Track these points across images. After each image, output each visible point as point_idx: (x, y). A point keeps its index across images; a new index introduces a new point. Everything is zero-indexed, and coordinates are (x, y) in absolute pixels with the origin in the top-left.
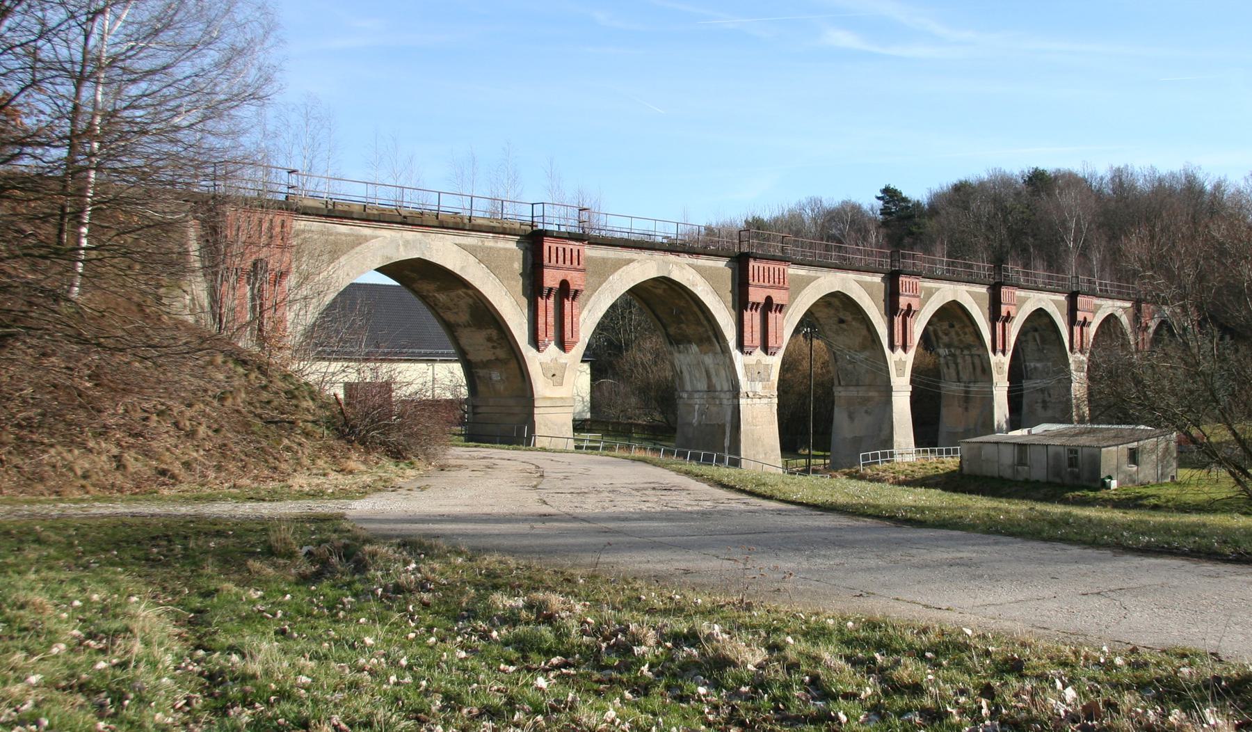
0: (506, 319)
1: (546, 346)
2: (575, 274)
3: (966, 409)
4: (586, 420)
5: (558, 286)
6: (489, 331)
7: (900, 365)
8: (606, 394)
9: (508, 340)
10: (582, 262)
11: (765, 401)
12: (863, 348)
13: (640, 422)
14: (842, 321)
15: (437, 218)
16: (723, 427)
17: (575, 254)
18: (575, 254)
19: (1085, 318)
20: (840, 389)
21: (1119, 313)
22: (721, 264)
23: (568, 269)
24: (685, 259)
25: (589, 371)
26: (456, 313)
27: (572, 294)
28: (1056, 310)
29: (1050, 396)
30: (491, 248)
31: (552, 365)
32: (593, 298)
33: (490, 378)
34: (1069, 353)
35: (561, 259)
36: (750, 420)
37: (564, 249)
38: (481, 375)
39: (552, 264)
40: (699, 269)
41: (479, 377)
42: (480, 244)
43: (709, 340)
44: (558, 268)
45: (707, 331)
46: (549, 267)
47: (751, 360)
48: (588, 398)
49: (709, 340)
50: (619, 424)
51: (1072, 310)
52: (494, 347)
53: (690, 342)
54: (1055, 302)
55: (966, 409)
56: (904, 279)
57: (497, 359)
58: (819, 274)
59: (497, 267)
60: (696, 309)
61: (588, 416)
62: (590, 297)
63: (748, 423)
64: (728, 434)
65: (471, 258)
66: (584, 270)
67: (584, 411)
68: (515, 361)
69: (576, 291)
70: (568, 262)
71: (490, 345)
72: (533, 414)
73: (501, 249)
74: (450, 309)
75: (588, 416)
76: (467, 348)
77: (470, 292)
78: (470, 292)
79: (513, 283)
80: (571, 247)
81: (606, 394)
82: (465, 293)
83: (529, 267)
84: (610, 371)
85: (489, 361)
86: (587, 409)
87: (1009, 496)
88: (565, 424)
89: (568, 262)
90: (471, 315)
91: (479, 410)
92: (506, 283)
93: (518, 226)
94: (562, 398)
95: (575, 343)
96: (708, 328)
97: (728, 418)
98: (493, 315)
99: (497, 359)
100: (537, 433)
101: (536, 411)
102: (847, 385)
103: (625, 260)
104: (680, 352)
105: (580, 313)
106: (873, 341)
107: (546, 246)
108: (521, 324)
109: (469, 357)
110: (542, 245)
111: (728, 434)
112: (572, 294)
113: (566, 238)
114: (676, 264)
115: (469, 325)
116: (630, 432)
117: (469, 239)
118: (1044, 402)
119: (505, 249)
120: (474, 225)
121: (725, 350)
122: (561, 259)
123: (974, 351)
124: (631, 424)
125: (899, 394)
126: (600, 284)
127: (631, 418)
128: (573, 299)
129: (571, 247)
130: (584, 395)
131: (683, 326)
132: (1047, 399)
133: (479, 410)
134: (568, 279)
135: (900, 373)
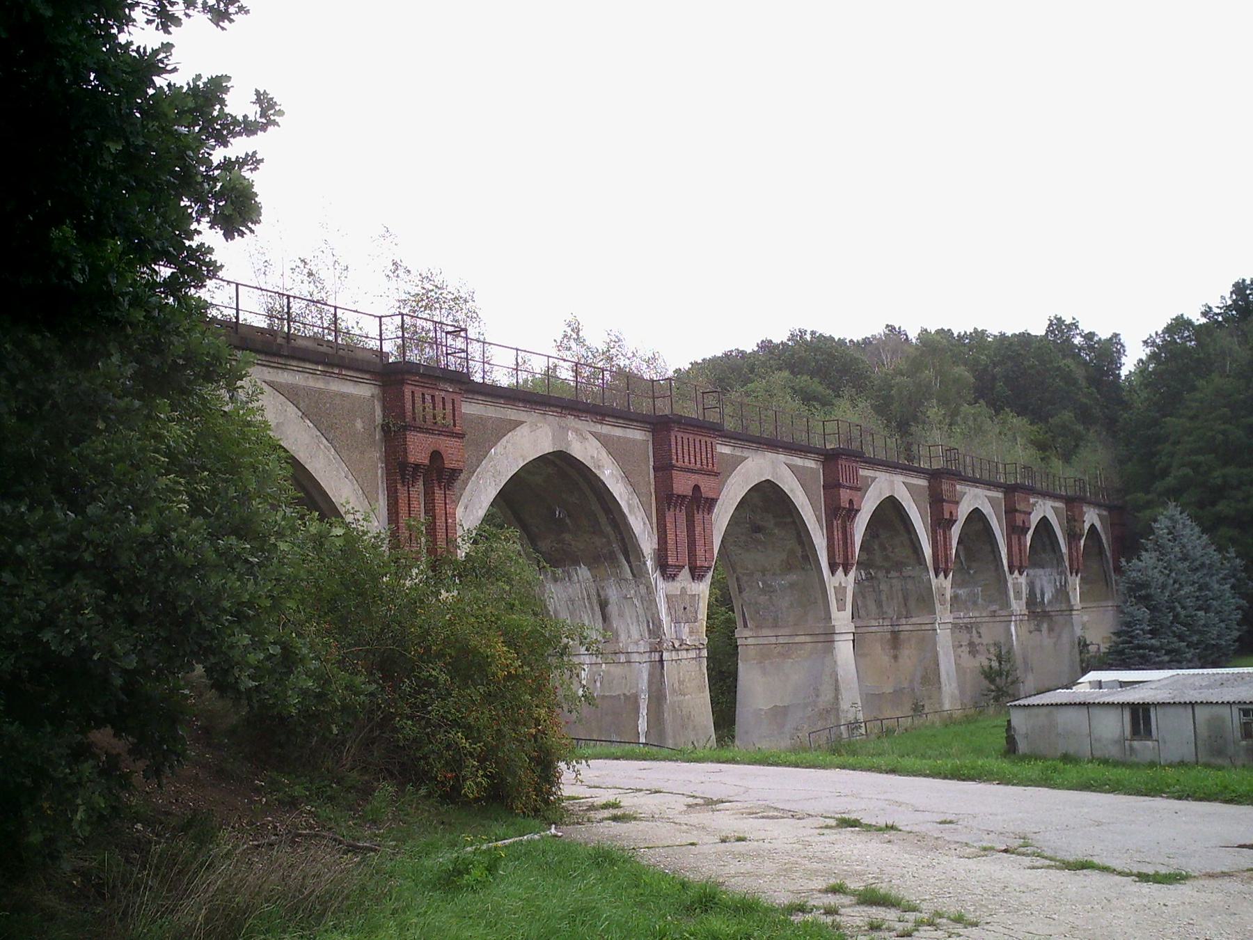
3: (896, 657)
7: (840, 590)
11: (693, 654)
12: (788, 567)
14: (757, 529)
15: (236, 332)
16: (634, 700)
19: (696, 488)
20: (747, 633)
21: (987, 510)
22: (637, 435)
24: (587, 425)
28: (604, 456)
29: (980, 637)
34: (1007, 573)
36: (676, 685)
39: (680, 464)
40: (605, 441)
43: (612, 558)
45: (609, 543)
47: (674, 587)
49: (612, 558)
51: (1011, 511)
53: (576, 562)
54: (990, 499)
55: (896, 657)
56: (844, 463)
58: (746, 453)
60: (595, 507)
63: (674, 691)
64: (644, 711)
65: (291, 409)
87: (1150, 717)
96: (612, 538)
97: (644, 684)
102: (759, 627)
104: (556, 580)
106: (806, 558)
107: (407, 391)
111: (644, 711)
114: (576, 431)
118: (971, 644)
120: (294, 348)
121: (639, 573)
123: (908, 571)
131: (567, 537)
132: (977, 641)
134: (442, 449)
135: (841, 608)
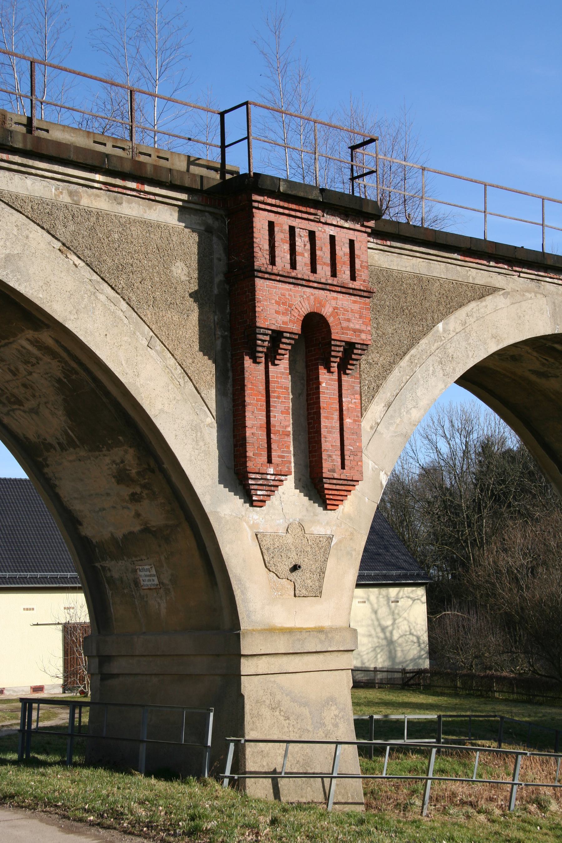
0: (151, 412)
1: (272, 488)
2: (345, 301)
4: (425, 671)
5: (297, 328)
6: (118, 453)
8: (451, 631)
9: (163, 471)
10: (362, 274)
13: (505, 674)
17: (343, 250)
18: (343, 250)
23: (324, 287)
25: (424, 599)
26: (35, 411)
27: (337, 352)
30: (99, 214)
31: (289, 539)
32: (396, 373)
33: (136, 583)
35: (303, 260)
37: (312, 235)
38: (116, 575)
41: (111, 581)
42: (65, 199)
44: (297, 282)
46: (271, 276)
48: (425, 638)
50: (472, 677)
52: (135, 498)
57: (146, 530)
59: (121, 268)
61: (426, 664)
62: (387, 369)
66: (367, 294)
67: (420, 657)
68: (189, 532)
69: (350, 347)
70: (324, 271)
71: (125, 491)
72: (239, 676)
73: (132, 221)
74: (19, 402)
75: (426, 664)
76: (77, 506)
77: (46, 337)
78: (46, 337)
79: (172, 316)
80: (332, 231)
81: (451, 631)
82: (36, 343)
83: (219, 278)
84: (454, 601)
85: (129, 537)
86: (424, 654)
88: (331, 701)
89: (324, 271)
90: (71, 413)
91: (115, 667)
92: (149, 315)
93: (181, 165)
94: (320, 630)
95: (352, 482)
98: (117, 405)
99: (146, 530)
100: (250, 734)
101: (247, 667)
103: (473, 287)
105: (363, 409)
108: (196, 428)
109: (87, 531)
110: (251, 216)
112: (337, 352)
113: (315, 204)
115: (72, 443)
116: (490, 689)
117: (29, 181)
119: (147, 224)
122: (303, 260)
124: (492, 677)
125: (262, 665)
126: (414, 341)
127: (490, 668)
128: (343, 368)
129: (332, 231)
130: (419, 633)
133: (115, 667)
134: (326, 311)
